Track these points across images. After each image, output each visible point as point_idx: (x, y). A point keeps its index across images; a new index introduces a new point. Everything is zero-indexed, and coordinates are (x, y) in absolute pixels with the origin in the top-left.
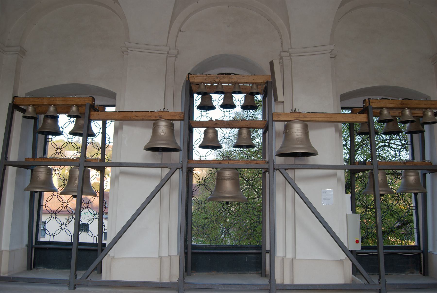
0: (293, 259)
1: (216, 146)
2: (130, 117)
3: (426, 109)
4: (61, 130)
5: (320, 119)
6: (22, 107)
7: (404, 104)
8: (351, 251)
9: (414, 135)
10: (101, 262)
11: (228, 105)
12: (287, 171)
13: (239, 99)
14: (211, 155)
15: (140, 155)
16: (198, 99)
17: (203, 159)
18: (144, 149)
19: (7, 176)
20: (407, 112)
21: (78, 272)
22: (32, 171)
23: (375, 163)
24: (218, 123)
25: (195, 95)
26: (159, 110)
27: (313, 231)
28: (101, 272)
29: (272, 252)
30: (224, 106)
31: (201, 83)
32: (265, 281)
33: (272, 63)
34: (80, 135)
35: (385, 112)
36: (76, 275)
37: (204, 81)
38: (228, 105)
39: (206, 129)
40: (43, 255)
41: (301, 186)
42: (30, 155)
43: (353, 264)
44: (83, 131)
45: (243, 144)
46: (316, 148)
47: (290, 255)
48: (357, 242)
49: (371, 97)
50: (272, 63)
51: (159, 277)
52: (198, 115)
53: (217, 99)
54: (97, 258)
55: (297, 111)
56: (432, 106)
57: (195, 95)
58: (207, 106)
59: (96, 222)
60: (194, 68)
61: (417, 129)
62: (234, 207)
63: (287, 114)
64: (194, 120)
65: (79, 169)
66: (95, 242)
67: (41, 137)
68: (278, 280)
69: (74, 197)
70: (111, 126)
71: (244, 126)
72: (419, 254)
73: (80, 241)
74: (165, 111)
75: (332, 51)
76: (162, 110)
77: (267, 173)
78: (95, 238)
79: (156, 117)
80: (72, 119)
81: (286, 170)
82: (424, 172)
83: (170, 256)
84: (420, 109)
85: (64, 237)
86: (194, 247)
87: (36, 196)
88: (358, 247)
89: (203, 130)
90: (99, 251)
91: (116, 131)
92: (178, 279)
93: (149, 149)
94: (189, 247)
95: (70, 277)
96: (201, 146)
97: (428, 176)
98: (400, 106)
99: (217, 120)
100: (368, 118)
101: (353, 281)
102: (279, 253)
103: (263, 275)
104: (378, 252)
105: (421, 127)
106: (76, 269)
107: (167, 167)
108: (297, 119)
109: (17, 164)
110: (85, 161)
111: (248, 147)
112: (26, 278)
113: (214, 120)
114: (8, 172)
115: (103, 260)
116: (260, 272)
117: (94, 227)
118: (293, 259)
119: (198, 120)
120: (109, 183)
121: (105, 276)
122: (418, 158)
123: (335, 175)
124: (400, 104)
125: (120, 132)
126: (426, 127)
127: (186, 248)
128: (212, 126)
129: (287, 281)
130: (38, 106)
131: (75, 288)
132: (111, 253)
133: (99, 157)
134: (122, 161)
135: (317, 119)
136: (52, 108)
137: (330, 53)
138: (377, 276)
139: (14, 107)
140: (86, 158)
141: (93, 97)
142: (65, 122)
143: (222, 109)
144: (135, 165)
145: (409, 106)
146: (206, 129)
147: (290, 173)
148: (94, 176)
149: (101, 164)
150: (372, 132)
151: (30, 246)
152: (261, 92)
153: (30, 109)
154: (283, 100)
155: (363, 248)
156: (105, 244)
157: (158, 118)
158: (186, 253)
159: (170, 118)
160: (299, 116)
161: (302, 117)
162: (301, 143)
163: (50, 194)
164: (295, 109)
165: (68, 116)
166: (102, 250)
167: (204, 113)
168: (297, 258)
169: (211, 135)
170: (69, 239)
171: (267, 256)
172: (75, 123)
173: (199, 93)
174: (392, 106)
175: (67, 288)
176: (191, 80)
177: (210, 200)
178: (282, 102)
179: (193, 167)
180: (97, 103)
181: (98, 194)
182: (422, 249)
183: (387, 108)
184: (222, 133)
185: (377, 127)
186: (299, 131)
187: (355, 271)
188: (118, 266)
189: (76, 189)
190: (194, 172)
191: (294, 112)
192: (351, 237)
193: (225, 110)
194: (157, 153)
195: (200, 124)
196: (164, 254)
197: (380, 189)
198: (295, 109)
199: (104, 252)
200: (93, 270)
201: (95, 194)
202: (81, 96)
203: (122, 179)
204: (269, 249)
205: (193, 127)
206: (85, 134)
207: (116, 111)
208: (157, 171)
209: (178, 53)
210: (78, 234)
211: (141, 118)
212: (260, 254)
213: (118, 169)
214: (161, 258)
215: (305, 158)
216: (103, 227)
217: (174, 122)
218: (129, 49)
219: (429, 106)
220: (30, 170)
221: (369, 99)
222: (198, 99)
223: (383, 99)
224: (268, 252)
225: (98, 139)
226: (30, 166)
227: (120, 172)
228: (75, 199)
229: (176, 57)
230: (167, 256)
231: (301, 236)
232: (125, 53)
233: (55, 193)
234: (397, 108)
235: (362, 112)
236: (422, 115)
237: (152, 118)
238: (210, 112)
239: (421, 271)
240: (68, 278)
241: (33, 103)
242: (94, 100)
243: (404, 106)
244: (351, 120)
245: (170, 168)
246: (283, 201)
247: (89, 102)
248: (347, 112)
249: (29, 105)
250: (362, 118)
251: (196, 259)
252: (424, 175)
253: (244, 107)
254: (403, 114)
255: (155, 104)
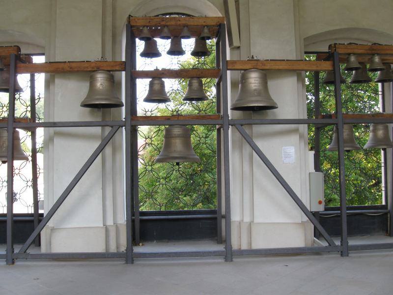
2: (63, 69)
5: (281, 67)
7: (373, 50)
8: (315, 214)
9: (386, 84)
10: (39, 235)
11: (176, 50)
12: (243, 126)
13: (188, 44)
15: (78, 114)
16: (140, 45)
17: (149, 114)
18: (81, 106)
20: (377, 59)
23: (340, 116)
25: (137, 40)
27: (271, 192)
29: (227, 216)
32: (220, 248)
35: (353, 59)
36: (13, 249)
37: (147, 24)
38: (176, 50)
39: (151, 79)
41: (260, 144)
43: (315, 228)
46: (275, 101)
47: (247, 219)
48: (320, 203)
49: (337, 42)
51: (104, 247)
52: (143, 64)
53: (163, 45)
54: (34, 230)
57: (137, 40)
58: (151, 52)
62: (196, 193)
63: (243, 62)
65: (7, 130)
66: (30, 212)
68: (235, 246)
71: (195, 76)
72: (386, 214)
74: (103, 61)
76: (100, 60)
77: (222, 129)
78: (30, 208)
79: (93, 68)
81: (242, 125)
86: (143, 214)
88: (321, 208)
89: (147, 81)
90: (36, 222)
91: (48, 84)
92: (125, 249)
94: (137, 214)
95: (7, 251)
98: (369, 52)
100: (334, 65)
102: (235, 217)
103: (220, 241)
104: (341, 213)
106: (13, 243)
107: (108, 126)
108: (255, 67)
110: (14, 122)
111: (198, 99)
113: (160, 69)
115: (41, 232)
116: (216, 238)
118: (250, 224)
119: (141, 69)
123: (296, 131)
124: (369, 50)
125: (51, 87)
127: (133, 214)
128: (157, 76)
129: (244, 247)
132: (50, 224)
133: (29, 115)
134: (56, 120)
135: (277, 67)
138: (340, 238)
141: (18, 46)
143: (170, 56)
144: (71, 125)
145: (378, 52)
146: (151, 79)
147: (247, 130)
148: (24, 135)
152: (212, 32)
156: (42, 215)
157: (95, 69)
158: (133, 221)
159: (109, 69)
160: (257, 64)
161: (261, 65)
164: (253, 56)
166: (40, 221)
167: (148, 60)
169: (157, 87)
171: (223, 221)
173: (141, 39)
174: (360, 51)
176: (132, 24)
177: (159, 161)
178: (239, 48)
180: (23, 51)
181: (30, 158)
184: (171, 85)
186: (257, 82)
187: (317, 234)
188: (60, 238)
189: (5, 154)
190: (139, 129)
191: (252, 59)
192: (314, 201)
193: (173, 57)
195: (144, 74)
197: (345, 145)
198: (253, 56)
199: (42, 224)
200: (31, 244)
201: (27, 159)
202: (4, 45)
203: (57, 141)
204: (224, 214)
206: (12, 90)
207: (46, 63)
208: (97, 130)
211: (76, 69)
212: (215, 219)
215: (264, 111)
221: (335, 44)
222: (140, 45)
223: (350, 44)
224: (224, 217)
225: (25, 95)
230: (112, 224)
234: (368, 54)
235: (327, 59)
238: (154, 59)
239: (387, 231)
242: (19, 49)
243: (373, 52)
244: (314, 68)
245: (112, 127)
246: (237, 161)
247: (13, 52)
248: (313, 58)
250: (327, 65)
251: (145, 228)
253: (195, 53)
254: (371, 61)
255: (92, 53)
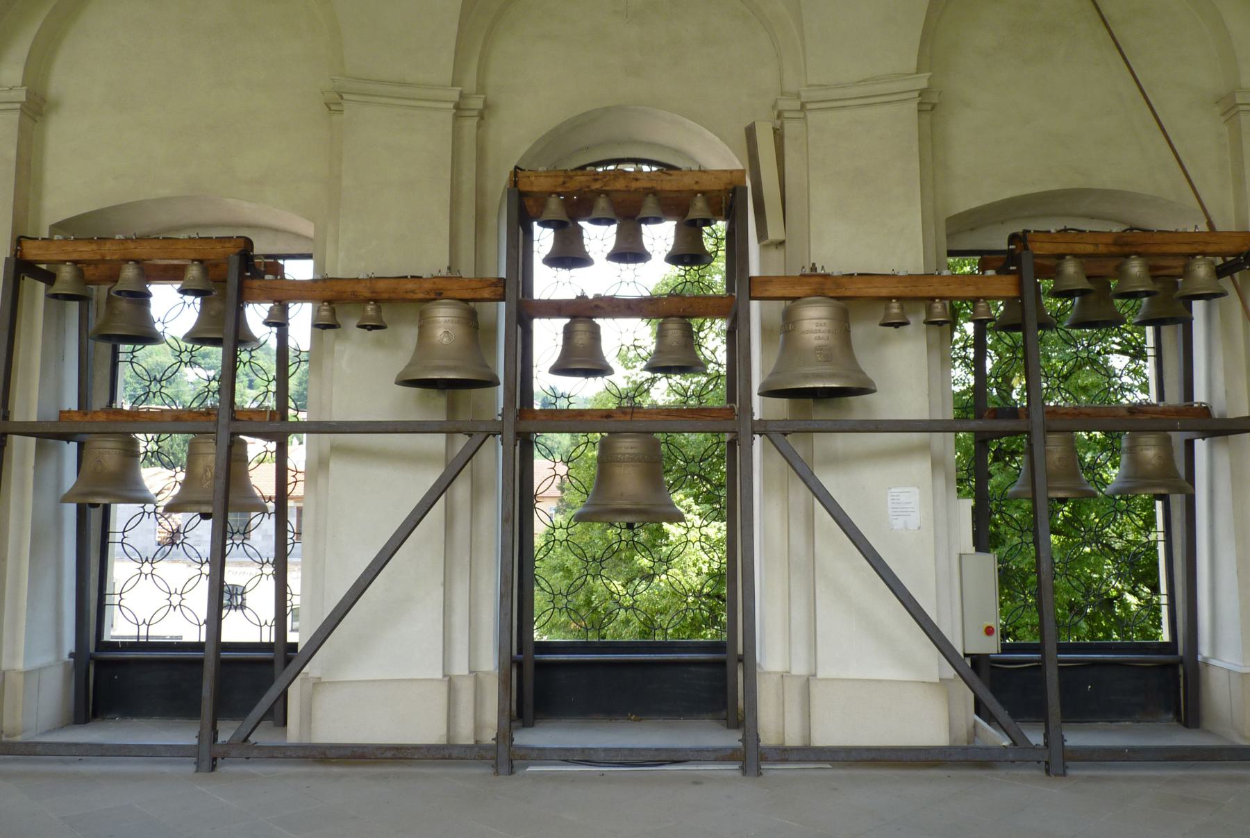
0: (808, 680)
1: (599, 369)
3: (1193, 255)
4: (159, 327)
6: (44, 267)
9: (1164, 329)
10: (285, 694)
11: (630, 251)
13: (660, 236)
14: (584, 392)
16: (544, 239)
19: (10, 462)
21: (221, 725)
22: (81, 447)
24: (601, 304)
25: (537, 228)
26: (436, 274)
28: (285, 723)
29: (747, 660)
30: (619, 255)
31: (550, 194)
33: (750, 133)
34: (216, 342)
37: (559, 190)
38: (629, 251)
39: (567, 321)
40: (116, 681)
41: (830, 481)
42: (71, 403)
44: (222, 331)
45: (676, 358)
46: (870, 373)
48: (989, 631)
49: (1032, 226)
50: (750, 133)
51: (444, 730)
52: (549, 283)
53: (599, 238)
55: (819, 271)
56: (1210, 249)
58: (569, 255)
59: (269, 585)
60: (531, 148)
61: (1170, 313)
64: (536, 297)
66: (266, 640)
67: (105, 348)
69: (205, 516)
70: (301, 316)
73: (226, 637)
75: (922, 93)
78: (266, 629)
80: (189, 299)
81: (785, 434)
82: (1188, 435)
83: (474, 673)
84: (1175, 255)
85: (186, 627)
87: (95, 516)
88: (991, 646)
90: (278, 665)
93: (407, 382)
94: (529, 650)
95: (199, 737)
96: (560, 369)
97: (1201, 446)
99: (598, 298)
101: (974, 731)
104: (1043, 660)
105: (1180, 305)
109: (40, 430)
111: (683, 370)
112: (76, 744)
113: (591, 297)
114: (11, 450)
116: (724, 713)
117: (262, 599)
118: (808, 680)
120: (300, 477)
121: (294, 733)
122: (1174, 397)
124: (1115, 244)
126: (1198, 307)
128: (582, 313)
129: (793, 739)
130: (89, 263)
131: (213, 768)
132: (312, 669)
133: (271, 403)
136: (129, 272)
137: (918, 100)
139: (22, 267)
140: (234, 411)
142: (173, 308)
144: (602, 756)
145: (1140, 250)
146: (567, 321)
149: (276, 426)
150: (1032, 323)
151: (78, 655)
153: (66, 272)
154: (781, 237)
155: (1005, 649)
157: (432, 296)
159: (466, 295)
162: (828, 359)
163: (135, 508)
165: (183, 291)
166: (288, 661)
167: (563, 273)
168: (820, 675)
169: (581, 338)
170: (193, 633)
172: (198, 307)
175: (192, 768)
176: (524, 186)
179: (532, 429)
181: (271, 506)
182: (1181, 652)
183: (1076, 256)
185: (1052, 305)
186: (823, 328)
188: (330, 708)
193: (624, 266)
194: (433, 392)
195: (553, 309)
196: (460, 668)
199: (293, 667)
203: (337, 467)
205: (532, 318)
206: (229, 342)
207: (314, 281)
208: (437, 442)
209: (487, 106)
210: (220, 619)
212: (722, 664)
213: (326, 438)
214: (450, 681)
216: (289, 597)
217: (477, 306)
218: (345, 96)
219: (1200, 248)
220: (75, 444)
222: (544, 239)
224: (741, 659)
225: (267, 360)
226: (76, 434)
227: (332, 448)
228: (207, 525)
229: (481, 116)
231: (830, 617)
232: (333, 107)
233: (149, 507)
236: (1180, 271)
237: (415, 296)
239: (1177, 713)
240: (195, 742)
241: (75, 256)
243: (1127, 249)
245: (470, 435)
248: (967, 267)
249: (64, 262)
252: (1190, 445)
